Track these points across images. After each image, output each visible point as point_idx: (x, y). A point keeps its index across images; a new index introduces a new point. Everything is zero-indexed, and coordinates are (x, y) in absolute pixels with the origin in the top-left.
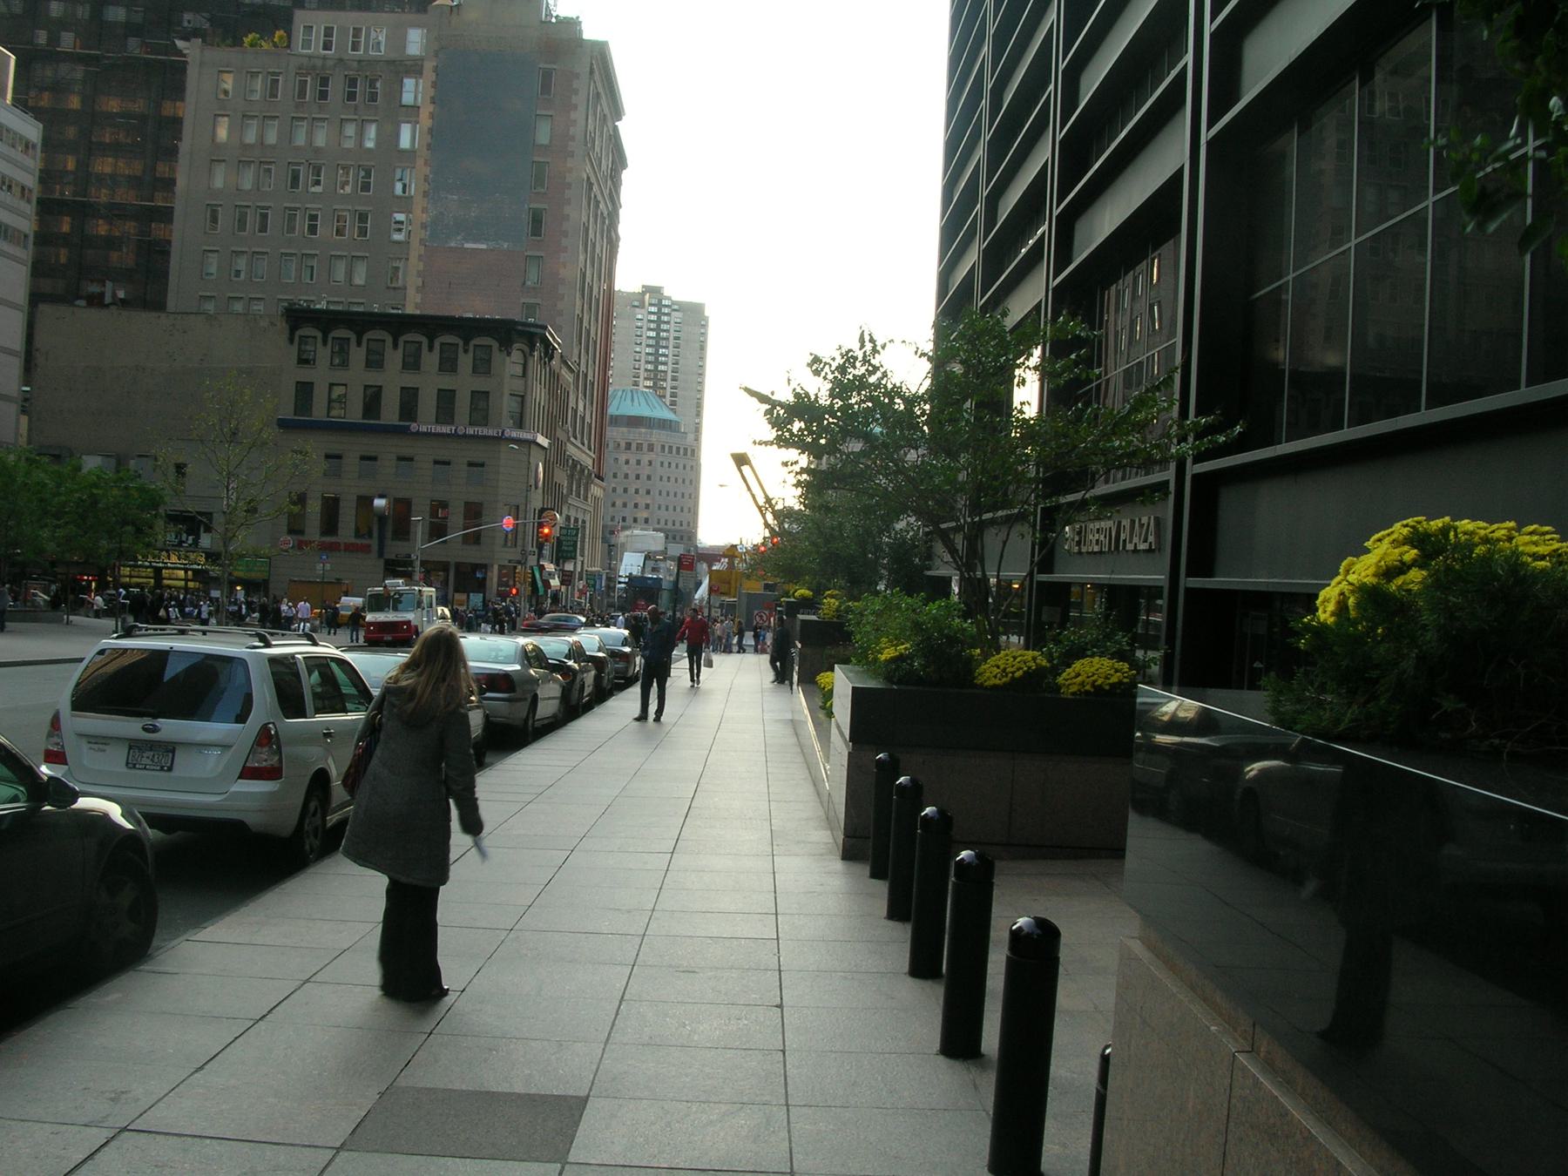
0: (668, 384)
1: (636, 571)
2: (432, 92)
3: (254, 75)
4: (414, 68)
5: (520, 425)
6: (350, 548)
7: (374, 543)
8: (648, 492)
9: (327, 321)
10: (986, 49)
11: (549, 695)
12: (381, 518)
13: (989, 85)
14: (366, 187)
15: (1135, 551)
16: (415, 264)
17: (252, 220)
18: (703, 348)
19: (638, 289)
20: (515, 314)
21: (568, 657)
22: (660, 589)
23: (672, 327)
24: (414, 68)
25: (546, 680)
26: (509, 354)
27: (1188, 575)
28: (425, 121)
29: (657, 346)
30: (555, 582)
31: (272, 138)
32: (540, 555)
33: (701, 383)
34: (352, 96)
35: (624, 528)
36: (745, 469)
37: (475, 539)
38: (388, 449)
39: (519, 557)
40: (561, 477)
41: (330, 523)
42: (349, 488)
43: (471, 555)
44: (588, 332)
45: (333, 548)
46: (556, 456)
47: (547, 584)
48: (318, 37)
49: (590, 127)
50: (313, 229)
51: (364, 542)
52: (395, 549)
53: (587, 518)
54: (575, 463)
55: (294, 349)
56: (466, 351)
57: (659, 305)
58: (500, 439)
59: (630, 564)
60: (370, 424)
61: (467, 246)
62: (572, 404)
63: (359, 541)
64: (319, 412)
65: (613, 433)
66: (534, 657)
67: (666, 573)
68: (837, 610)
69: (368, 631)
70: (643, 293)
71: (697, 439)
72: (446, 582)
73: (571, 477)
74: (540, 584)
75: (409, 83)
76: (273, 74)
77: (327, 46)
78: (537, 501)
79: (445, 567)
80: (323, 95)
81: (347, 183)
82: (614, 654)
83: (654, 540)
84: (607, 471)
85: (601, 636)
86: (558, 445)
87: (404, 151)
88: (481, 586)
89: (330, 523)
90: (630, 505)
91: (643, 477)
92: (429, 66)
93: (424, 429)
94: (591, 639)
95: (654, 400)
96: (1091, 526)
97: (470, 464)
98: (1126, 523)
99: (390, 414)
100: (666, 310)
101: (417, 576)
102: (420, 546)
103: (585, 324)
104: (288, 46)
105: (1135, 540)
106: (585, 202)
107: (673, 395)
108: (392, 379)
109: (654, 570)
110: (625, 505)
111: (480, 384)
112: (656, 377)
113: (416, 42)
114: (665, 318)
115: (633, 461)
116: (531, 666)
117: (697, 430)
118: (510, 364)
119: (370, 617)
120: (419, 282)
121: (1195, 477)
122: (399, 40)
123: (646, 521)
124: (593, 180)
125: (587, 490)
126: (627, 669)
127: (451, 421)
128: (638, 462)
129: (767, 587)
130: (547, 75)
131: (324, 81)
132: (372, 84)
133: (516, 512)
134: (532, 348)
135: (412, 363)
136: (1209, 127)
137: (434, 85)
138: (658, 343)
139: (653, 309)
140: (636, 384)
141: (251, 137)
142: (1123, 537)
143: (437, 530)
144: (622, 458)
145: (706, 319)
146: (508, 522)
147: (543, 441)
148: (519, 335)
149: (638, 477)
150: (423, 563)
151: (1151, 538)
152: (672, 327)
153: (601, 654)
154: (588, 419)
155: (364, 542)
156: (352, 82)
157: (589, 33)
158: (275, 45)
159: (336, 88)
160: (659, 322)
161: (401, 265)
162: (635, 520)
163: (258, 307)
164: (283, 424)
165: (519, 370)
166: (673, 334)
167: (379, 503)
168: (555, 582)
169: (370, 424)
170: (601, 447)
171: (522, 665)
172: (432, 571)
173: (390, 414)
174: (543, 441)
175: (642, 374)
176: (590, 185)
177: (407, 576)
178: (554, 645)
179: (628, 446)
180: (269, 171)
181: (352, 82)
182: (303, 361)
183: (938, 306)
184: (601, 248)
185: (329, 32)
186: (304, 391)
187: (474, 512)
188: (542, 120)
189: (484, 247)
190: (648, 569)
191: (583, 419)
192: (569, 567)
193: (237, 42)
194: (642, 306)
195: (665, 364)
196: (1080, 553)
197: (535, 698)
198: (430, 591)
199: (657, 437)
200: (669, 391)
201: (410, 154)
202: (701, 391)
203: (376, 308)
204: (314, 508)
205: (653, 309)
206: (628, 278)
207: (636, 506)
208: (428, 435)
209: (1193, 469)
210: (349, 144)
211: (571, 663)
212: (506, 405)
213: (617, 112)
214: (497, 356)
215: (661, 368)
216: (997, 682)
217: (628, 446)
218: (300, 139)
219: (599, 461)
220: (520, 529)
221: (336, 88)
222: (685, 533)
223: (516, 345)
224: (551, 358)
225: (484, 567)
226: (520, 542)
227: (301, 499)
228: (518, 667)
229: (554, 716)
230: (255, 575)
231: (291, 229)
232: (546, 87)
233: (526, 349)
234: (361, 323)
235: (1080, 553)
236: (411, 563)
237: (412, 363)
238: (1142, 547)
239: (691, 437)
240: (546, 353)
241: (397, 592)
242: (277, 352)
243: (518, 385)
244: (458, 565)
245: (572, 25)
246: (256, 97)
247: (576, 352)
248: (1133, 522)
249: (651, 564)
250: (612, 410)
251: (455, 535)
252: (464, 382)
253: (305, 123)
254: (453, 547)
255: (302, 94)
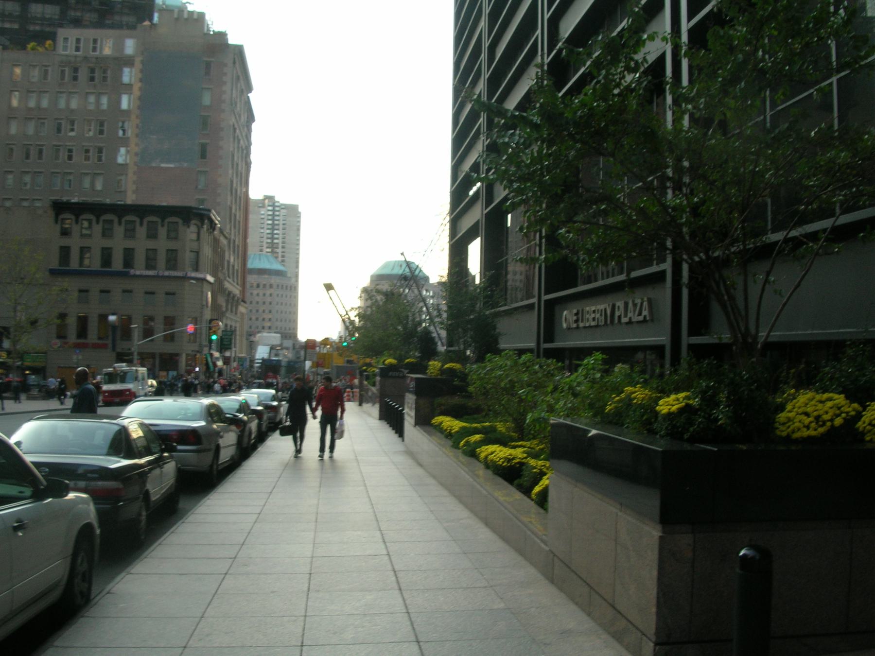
0: (279, 250)
1: (266, 356)
2: (140, 75)
3: (35, 66)
4: (129, 62)
5: (197, 269)
6: (96, 346)
7: (109, 342)
8: (270, 312)
9: (78, 209)
10: (483, 24)
11: (229, 439)
12: (114, 327)
13: (486, 44)
14: (101, 132)
15: (630, 322)
16: (131, 177)
17: (33, 153)
18: (298, 229)
19: (261, 197)
20: (193, 204)
21: (240, 411)
22: (280, 366)
23: (281, 218)
24: (129, 62)
25: (227, 431)
26: (189, 227)
27: (691, 333)
28: (136, 92)
29: (273, 229)
30: (220, 363)
31: (45, 103)
32: (210, 348)
33: (298, 249)
34: (92, 79)
35: (259, 332)
36: (331, 292)
37: (170, 338)
38: (117, 286)
39: (197, 349)
40: (222, 301)
41: (82, 332)
42: (93, 310)
43: (169, 348)
44: (235, 216)
45: (84, 346)
46: (218, 289)
47: (215, 365)
48: (72, 43)
49: (234, 96)
50: (70, 158)
51: (104, 342)
52: (122, 346)
53: (238, 325)
54: (230, 293)
55: (58, 228)
56: (163, 226)
57: (274, 206)
58: (185, 278)
59: (262, 352)
60: (106, 269)
61: (163, 165)
62: (227, 258)
63: (100, 342)
64: (74, 264)
65: (251, 279)
66: (214, 413)
67: (286, 356)
68: (440, 370)
69: (105, 397)
70: (264, 199)
71: (297, 281)
72: (154, 365)
73: (227, 301)
74: (211, 364)
75: (126, 70)
76: (46, 66)
77: (77, 49)
78: (208, 315)
79: (153, 356)
80: (75, 78)
81: (90, 130)
82: (268, 407)
83: (274, 338)
84: (247, 300)
85: (259, 395)
86: (219, 282)
87: (124, 111)
88: (175, 367)
89: (82, 332)
90: (260, 319)
91: (267, 303)
92: (138, 61)
93: (138, 273)
94: (253, 396)
95: (272, 259)
96: (588, 308)
97: (167, 294)
98: (620, 304)
99: (117, 264)
100: (277, 209)
101: (135, 361)
102: (137, 342)
103: (233, 211)
104: (54, 50)
105: (629, 315)
106: (232, 139)
107: (283, 256)
108: (118, 243)
109: (276, 355)
110: (257, 319)
111: (172, 245)
112: (273, 246)
113: (130, 46)
114: (277, 213)
115: (261, 294)
116: (215, 422)
117: (297, 276)
118: (190, 233)
119: (105, 387)
120: (134, 187)
121: (545, 301)
122: (119, 46)
123: (270, 328)
124: (236, 126)
125: (237, 309)
126: (276, 416)
127: (154, 268)
128: (264, 295)
129: (349, 362)
130: (208, 65)
131: (76, 70)
132: (105, 72)
133: (195, 321)
134: (203, 224)
135: (130, 233)
136: (690, 19)
137: (141, 71)
138: (273, 227)
139: (270, 208)
140: (261, 251)
141: (32, 104)
142: (617, 314)
143: (148, 332)
144: (255, 292)
145: (300, 213)
146: (190, 328)
147: (210, 278)
148: (194, 216)
149: (264, 303)
150: (139, 354)
151: (645, 313)
152: (281, 218)
153: (260, 408)
154: (236, 267)
155: (104, 342)
156: (92, 71)
157: (232, 40)
158: (46, 49)
159: (83, 74)
160: (273, 215)
161: (123, 178)
162: (263, 328)
163: (38, 204)
164: (53, 272)
165: (194, 236)
166: (281, 222)
167: (112, 318)
168: (220, 363)
169: (106, 269)
170: (244, 284)
171: (207, 422)
172: (144, 358)
173: (117, 264)
174: (210, 278)
175: (265, 245)
176: (235, 129)
177: (130, 362)
178: (229, 402)
179: (258, 286)
180: (43, 123)
181: (92, 71)
182: (65, 233)
183: (452, 186)
184: (242, 167)
185: (78, 40)
186: (65, 252)
187: (170, 322)
188: (206, 82)
189: (172, 166)
190: (273, 354)
191: (233, 266)
192: (227, 354)
193: (24, 48)
194: (264, 207)
195: (277, 239)
196: (578, 328)
197: (218, 448)
198: (143, 370)
199: (275, 280)
200: (280, 255)
201: (127, 113)
202: (298, 254)
203: (108, 201)
204: (72, 321)
205: (270, 208)
206: (256, 192)
207: (264, 319)
208: (141, 276)
209: (545, 297)
210: (92, 107)
211: (241, 416)
212: (188, 257)
213: (249, 88)
214: (181, 228)
215: (276, 241)
216: (812, 433)
217: (258, 286)
218: (62, 104)
219: (243, 292)
220: (198, 331)
221: (83, 74)
222: (289, 334)
223: (193, 222)
224: (214, 229)
225: (177, 355)
226: (198, 340)
227: (63, 316)
228: (203, 423)
229: (232, 458)
230: (38, 364)
231: (57, 158)
232: (207, 73)
233: (199, 224)
234: (97, 210)
235: (578, 328)
236: (132, 354)
237: (130, 233)
238: (636, 319)
239: (293, 280)
240: (211, 227)
241: (122, 371)
242: (47, 229)
243: (195, 246)
244: (161, 355)
245: (222, 36)
246: (35, 80)
247: (228, 227)
248: (626, 304)
249: (274, 352)
250: (252, 264)
251: (159, 335)
252: (162, 244)
253: (64, 95)
254: (158, 343)
255: (63, 78)
